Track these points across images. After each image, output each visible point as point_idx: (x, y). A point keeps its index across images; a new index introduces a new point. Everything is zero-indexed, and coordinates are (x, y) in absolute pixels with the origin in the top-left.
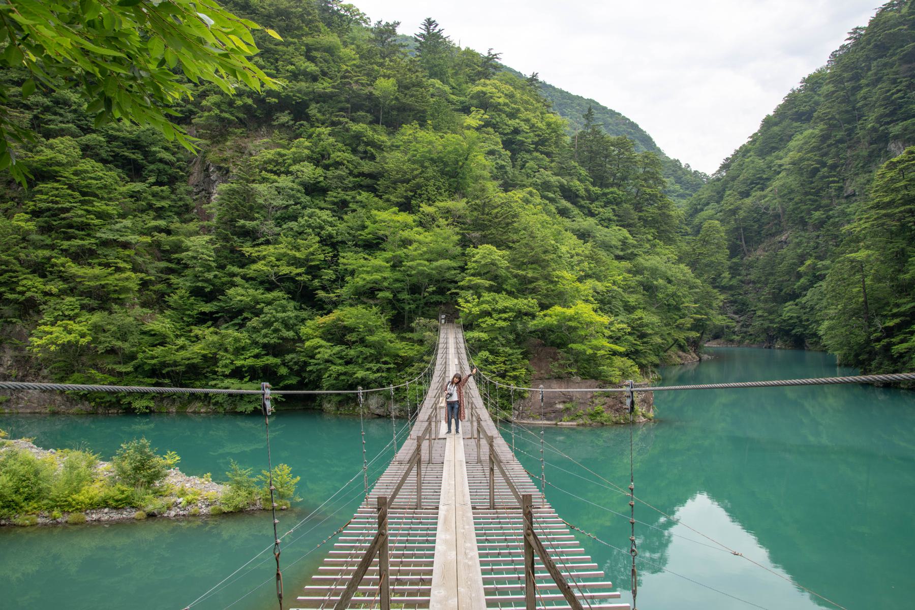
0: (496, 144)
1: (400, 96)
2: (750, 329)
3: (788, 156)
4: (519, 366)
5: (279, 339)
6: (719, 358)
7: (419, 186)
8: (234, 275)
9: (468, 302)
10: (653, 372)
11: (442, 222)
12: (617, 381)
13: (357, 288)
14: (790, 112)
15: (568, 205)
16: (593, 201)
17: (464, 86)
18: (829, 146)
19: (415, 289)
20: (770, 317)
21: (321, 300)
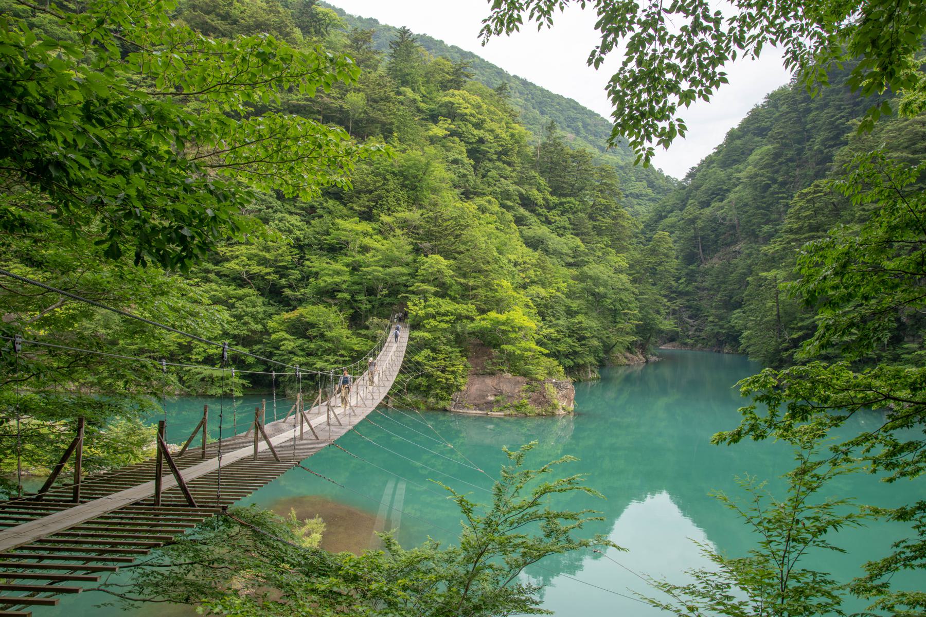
0: (461, 153)
1: (368, 109)
2: (702, 334)
3: (745, 171)
4: (455, 363)
5: (248, 331)
6: (670, 359)
7: (380, 197)
8: (207, 271)
9: (416, 305)
10: (593, 371)
11: (398, 232)
12: (542, 378)
13: (319, 289)
14: (752, 127)
15: (526, 213)
16: (550, 209)
17: (435, 94)
18: (780, 164)
19: (371, 291)
20: (721, 323)
21: (287, 297)
